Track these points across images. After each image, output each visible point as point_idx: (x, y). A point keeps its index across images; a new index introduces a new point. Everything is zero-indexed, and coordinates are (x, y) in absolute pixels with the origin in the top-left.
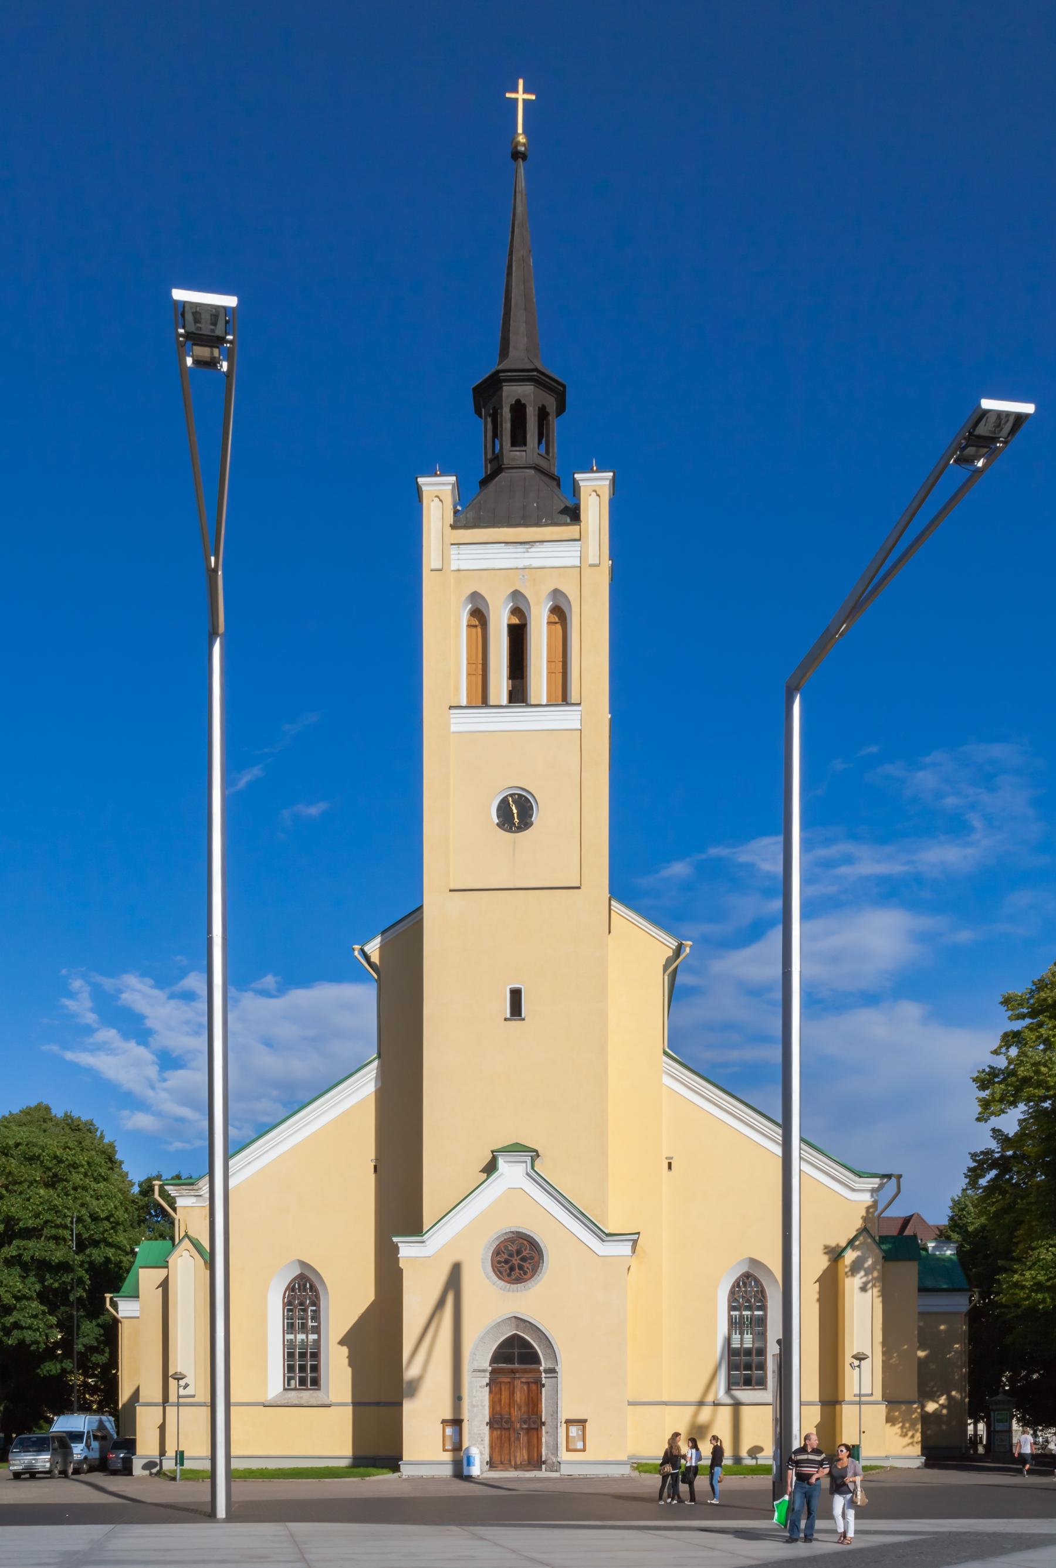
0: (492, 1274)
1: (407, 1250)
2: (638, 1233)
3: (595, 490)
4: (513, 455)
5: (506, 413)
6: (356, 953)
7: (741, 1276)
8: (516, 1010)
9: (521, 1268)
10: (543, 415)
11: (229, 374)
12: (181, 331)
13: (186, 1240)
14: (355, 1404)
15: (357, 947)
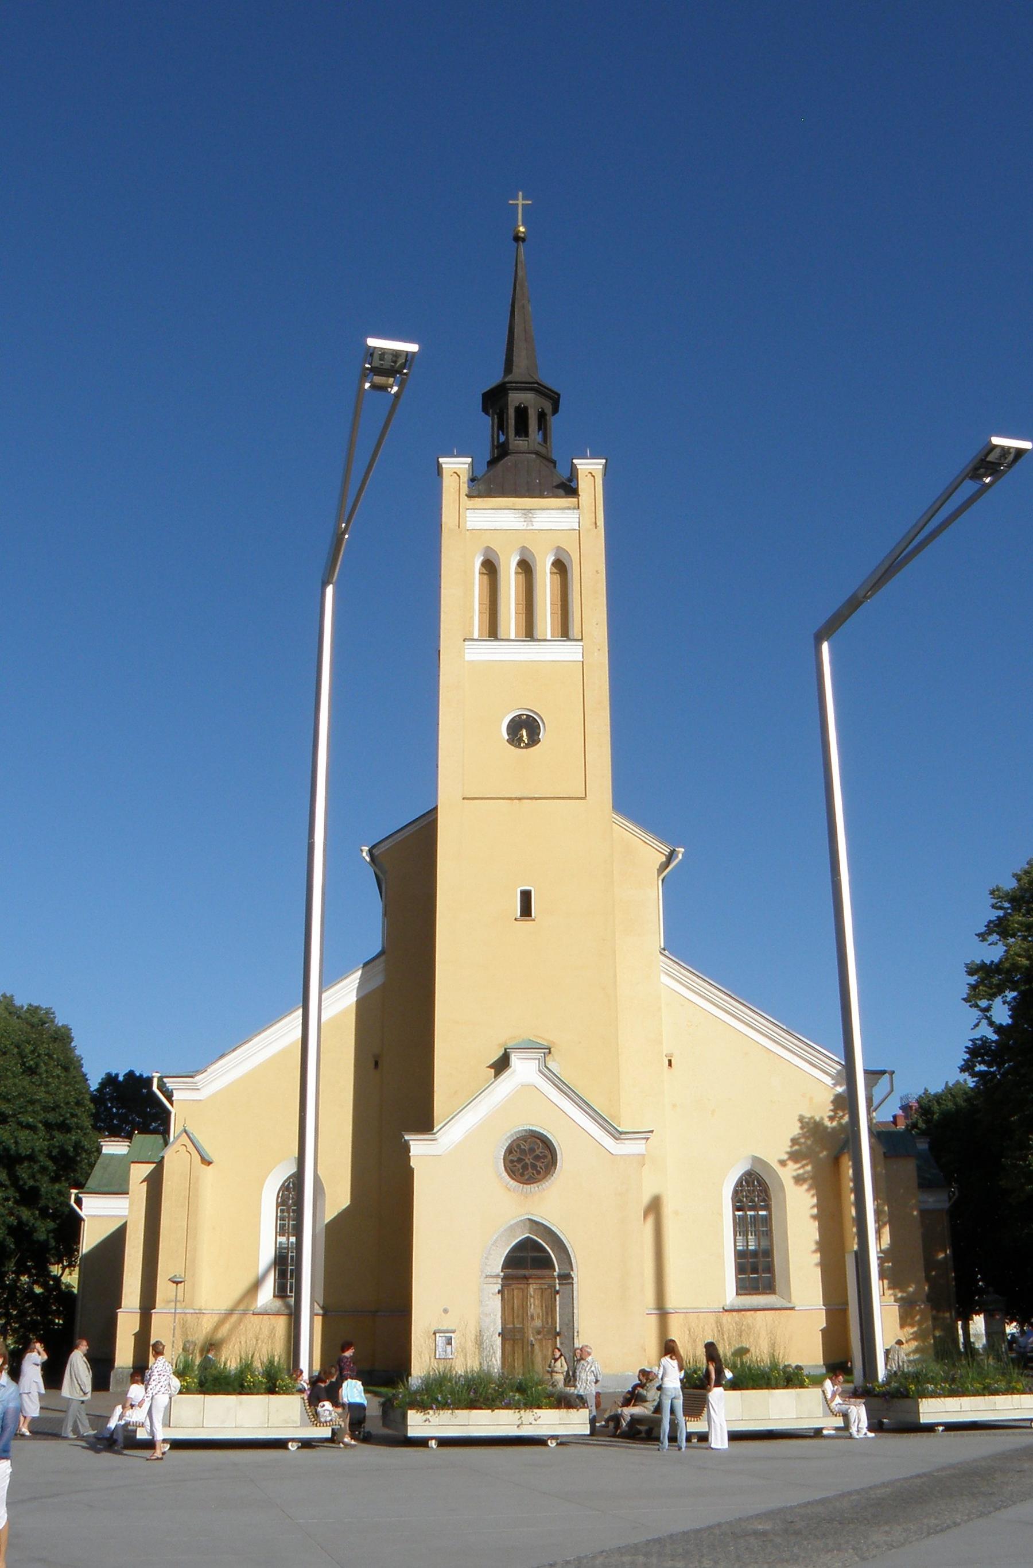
0: (505, 1174)
2: (652, 1131)
3: (590, 470)
4: (517, 443)
5: (511, 412)
6: (364, 854)
7: (743, 1175)
8: (526, 910)
9: (534, 1167)
10: (542, 416)
11: (397, 395)
12: (367, 366)
14: (504, 1278)
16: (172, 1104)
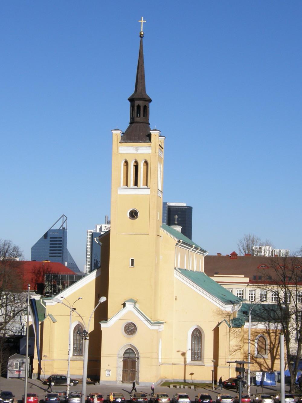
1: (103, 325)
4: (137, 119)
8: (132, 265)
13: (49, 316)
15: (95, 239)
16: (46, 307)
